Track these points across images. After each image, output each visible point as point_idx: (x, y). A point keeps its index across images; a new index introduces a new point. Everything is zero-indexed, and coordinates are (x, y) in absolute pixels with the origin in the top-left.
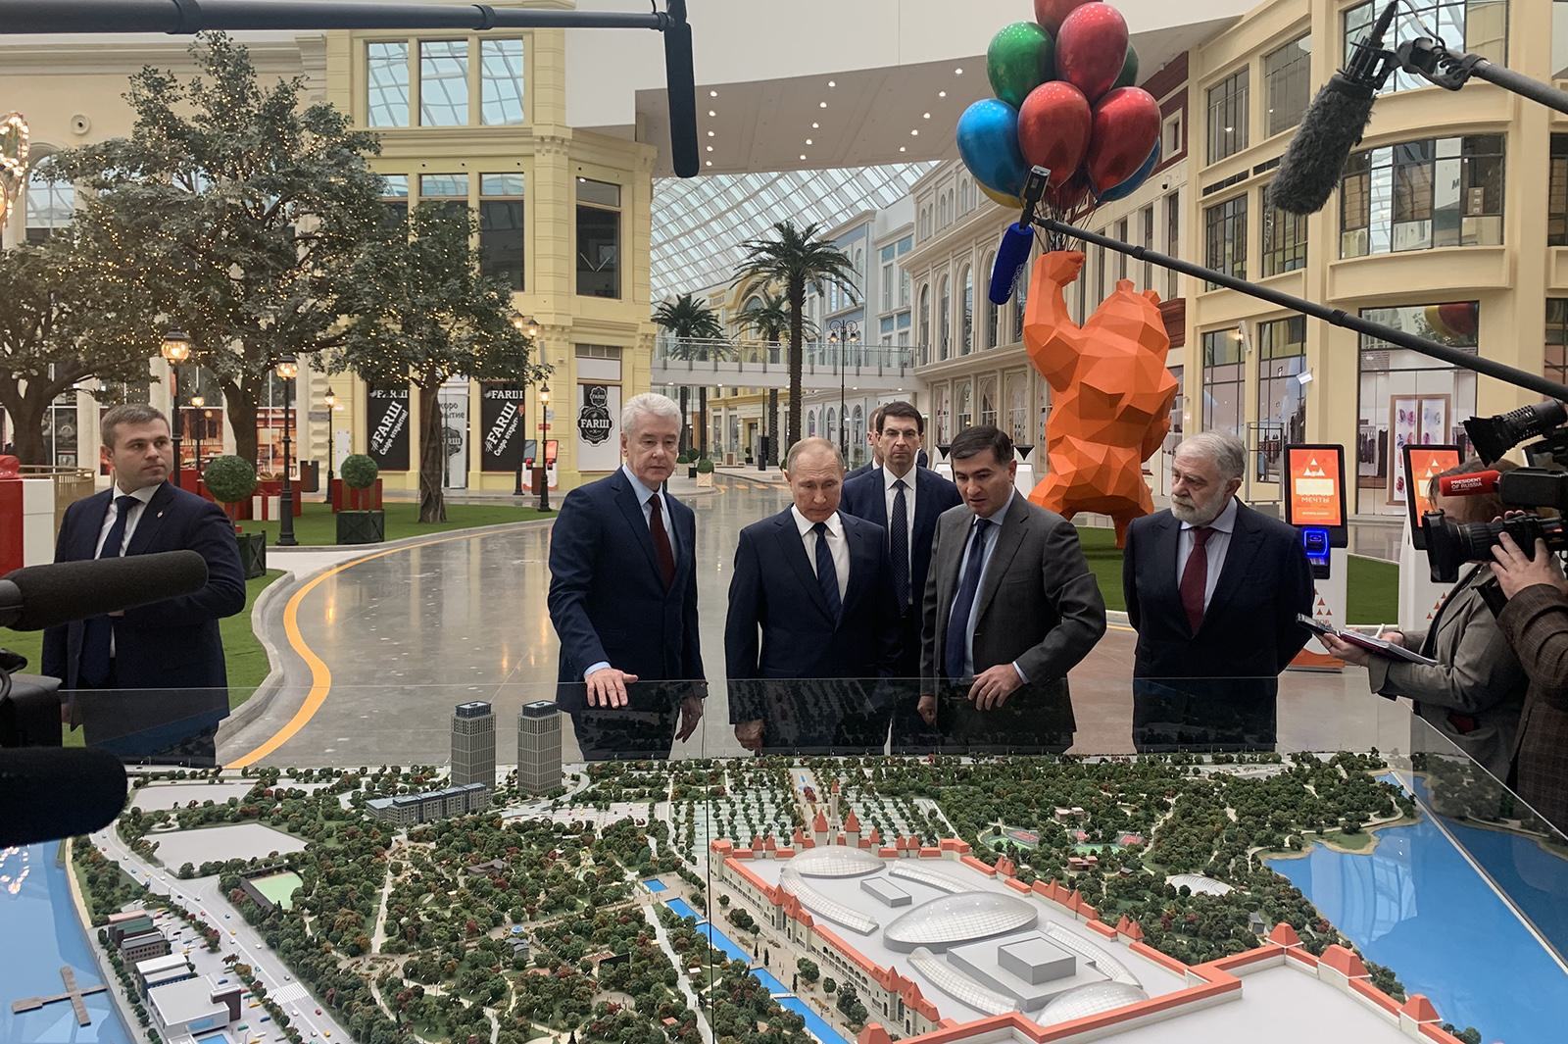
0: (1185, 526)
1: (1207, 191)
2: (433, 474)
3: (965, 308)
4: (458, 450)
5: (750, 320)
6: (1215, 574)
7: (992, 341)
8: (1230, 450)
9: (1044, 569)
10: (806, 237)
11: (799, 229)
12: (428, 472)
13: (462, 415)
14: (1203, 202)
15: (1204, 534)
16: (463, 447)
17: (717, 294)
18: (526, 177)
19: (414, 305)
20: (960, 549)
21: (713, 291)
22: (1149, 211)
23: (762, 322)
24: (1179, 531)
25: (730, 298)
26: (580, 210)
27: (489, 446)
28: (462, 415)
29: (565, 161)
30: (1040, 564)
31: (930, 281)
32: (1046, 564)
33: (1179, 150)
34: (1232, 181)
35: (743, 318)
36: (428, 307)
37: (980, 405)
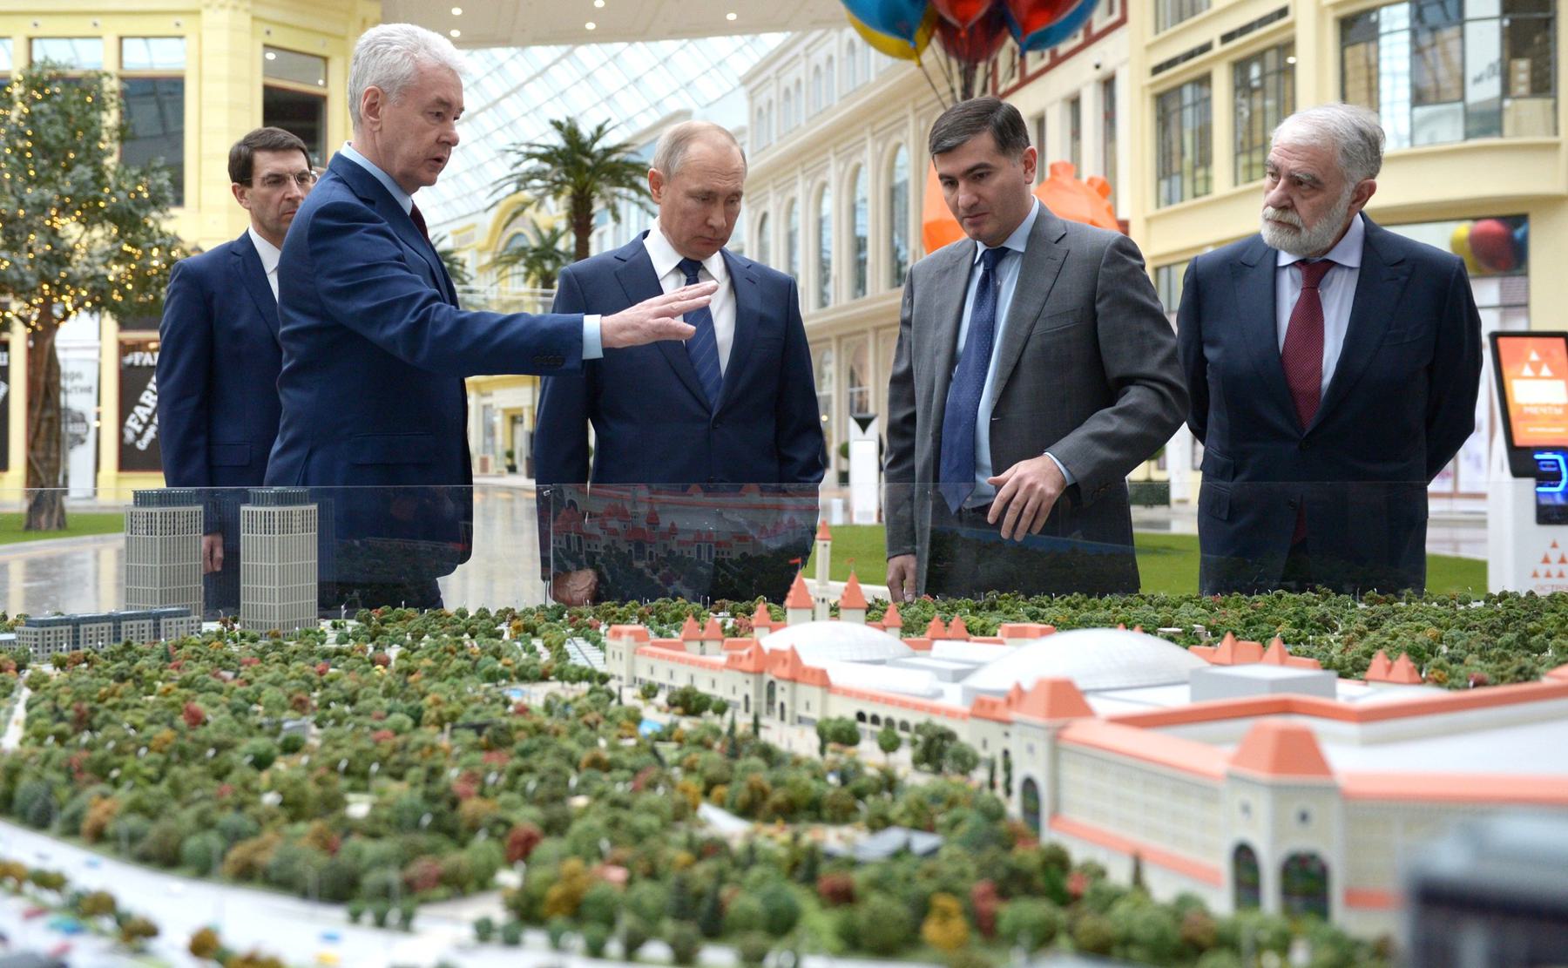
0: (1285, 259)
1: (1157, 70)
2: (47, 458)
3: (820, 250)
4: (83, 442)
5: (513, 262)
6: (1337, 333)
7: (860, 284)
8: (1362, 133)
9: (1099, 307)
10: (595, 139)
11: (586, 131)
12: (41, 454)
13: (89, 390)
14: (1152, 86)
15: (1315, 269)
16: (91, 438)
17: (463, 230)
18: (190, 42)
19: (21, 203)
20: (956, 304)
21: (458, 225)
22: (1075, 103)
23: (530, 265)
24: (1276, 269)
25: (481, 239)
26: (268, 90)
27: (130, 436)
28: (89, 390)
29: (246, 20)
30: (1092, 299)
31: (770, 207)
32: (1103, 296)
33: (1116, 16)
34: (1190, 55)
35: (507, 258)
36: (42, 207)
37: (845, 380)
